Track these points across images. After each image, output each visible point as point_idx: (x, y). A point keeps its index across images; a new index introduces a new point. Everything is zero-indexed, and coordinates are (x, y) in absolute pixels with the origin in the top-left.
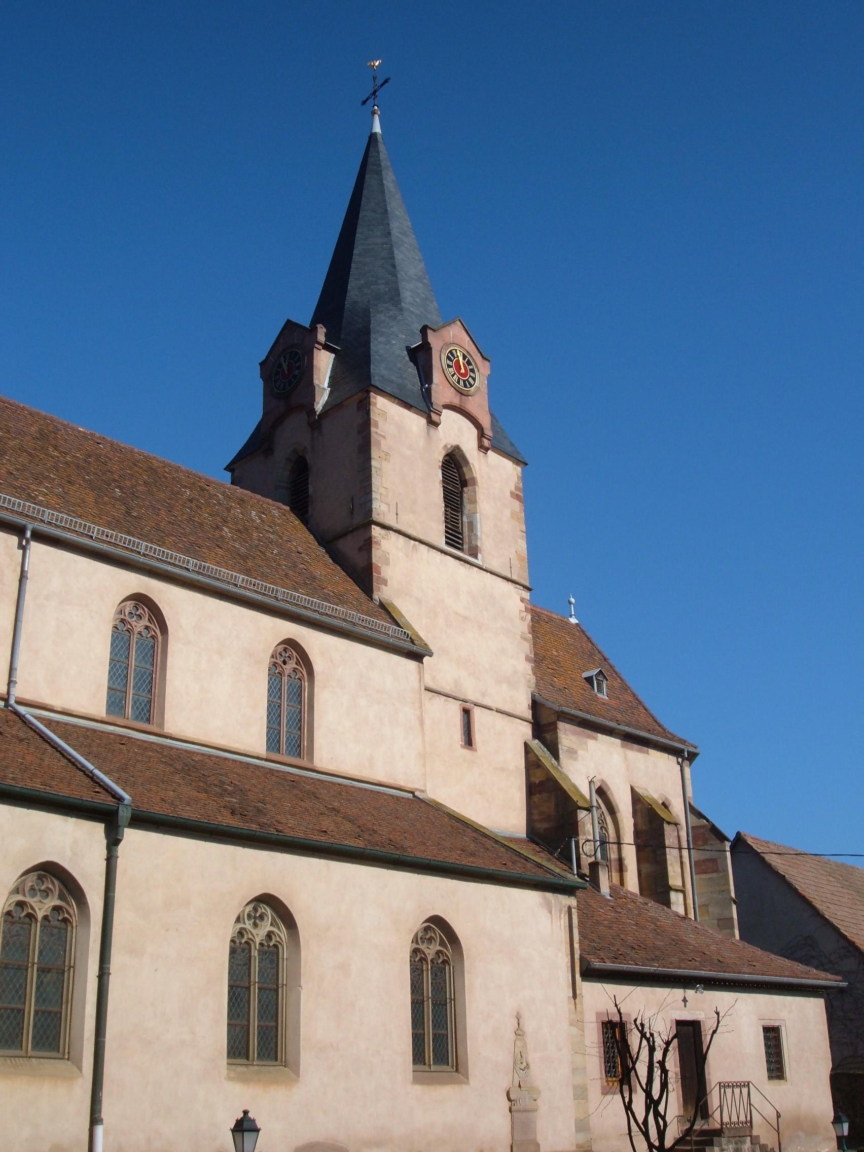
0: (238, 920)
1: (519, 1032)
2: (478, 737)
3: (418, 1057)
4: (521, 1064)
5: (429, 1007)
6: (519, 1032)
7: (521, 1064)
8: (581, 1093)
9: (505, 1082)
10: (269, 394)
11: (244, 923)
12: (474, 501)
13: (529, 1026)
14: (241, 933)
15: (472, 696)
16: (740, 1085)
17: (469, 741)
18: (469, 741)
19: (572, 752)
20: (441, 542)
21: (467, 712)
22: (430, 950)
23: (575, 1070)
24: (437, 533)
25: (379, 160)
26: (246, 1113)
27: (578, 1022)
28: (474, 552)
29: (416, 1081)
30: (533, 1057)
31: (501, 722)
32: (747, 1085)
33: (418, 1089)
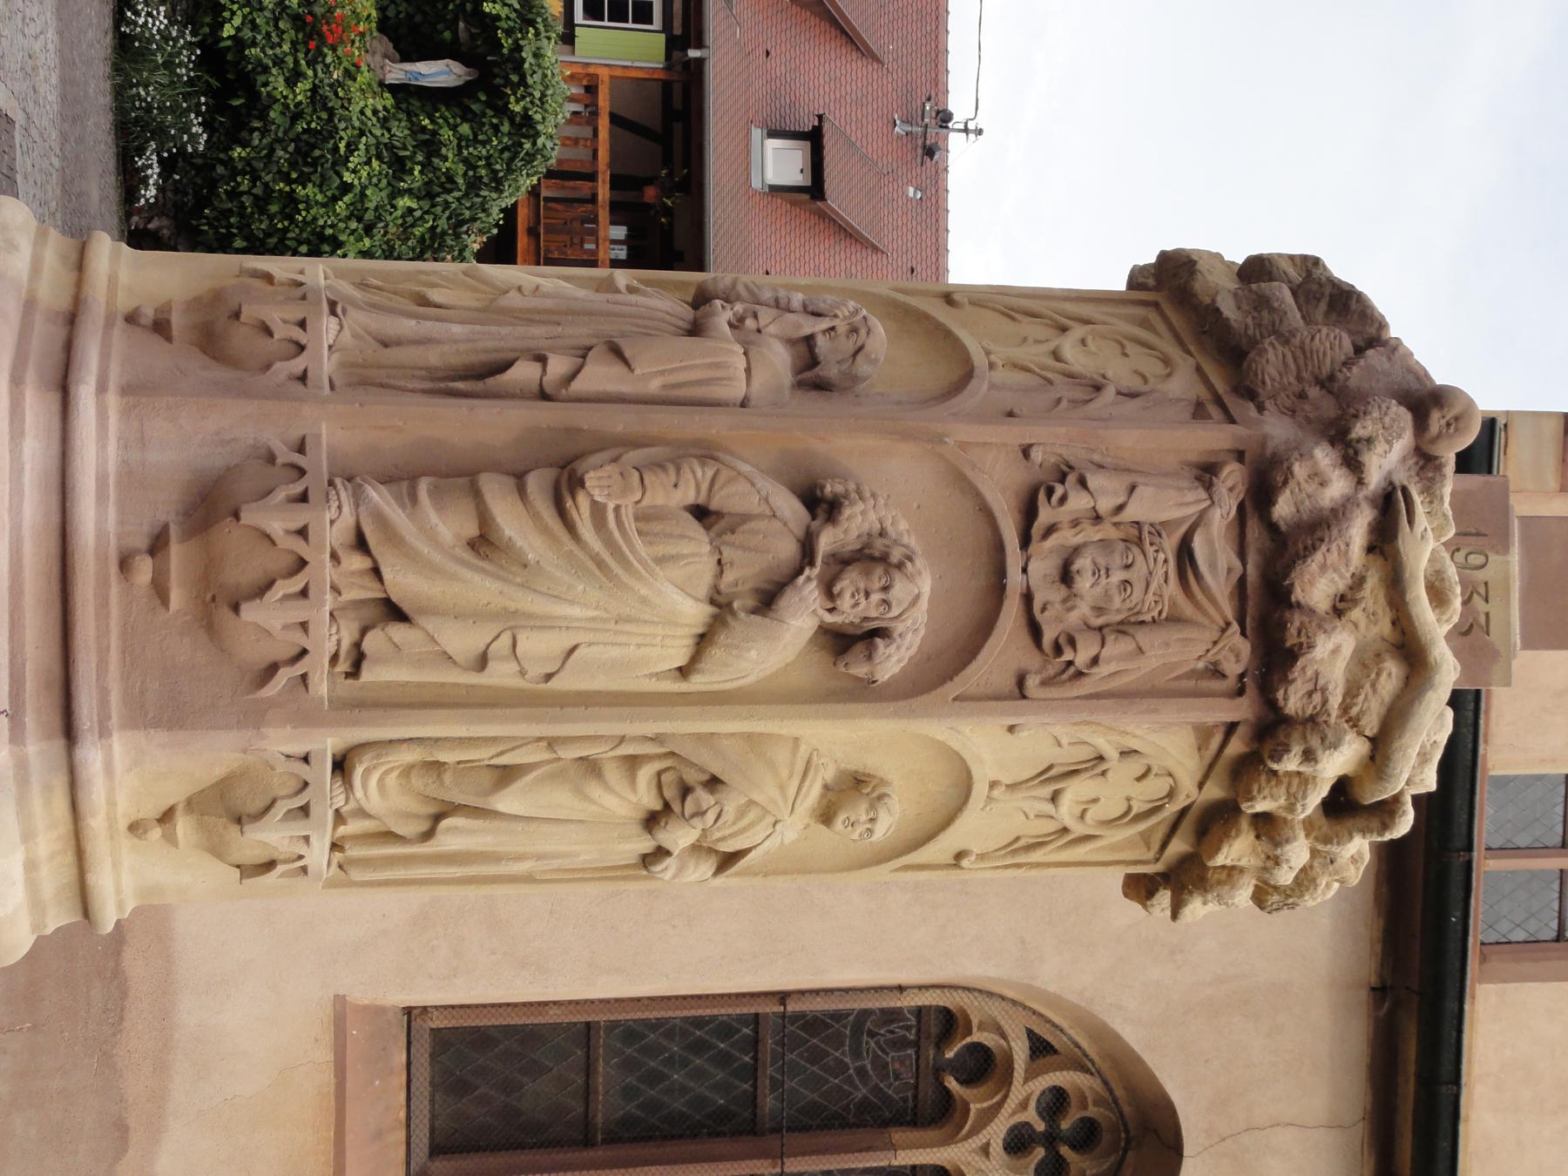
11: (1030, 1076)
14: (984, 1066)
29: (341, 1012)
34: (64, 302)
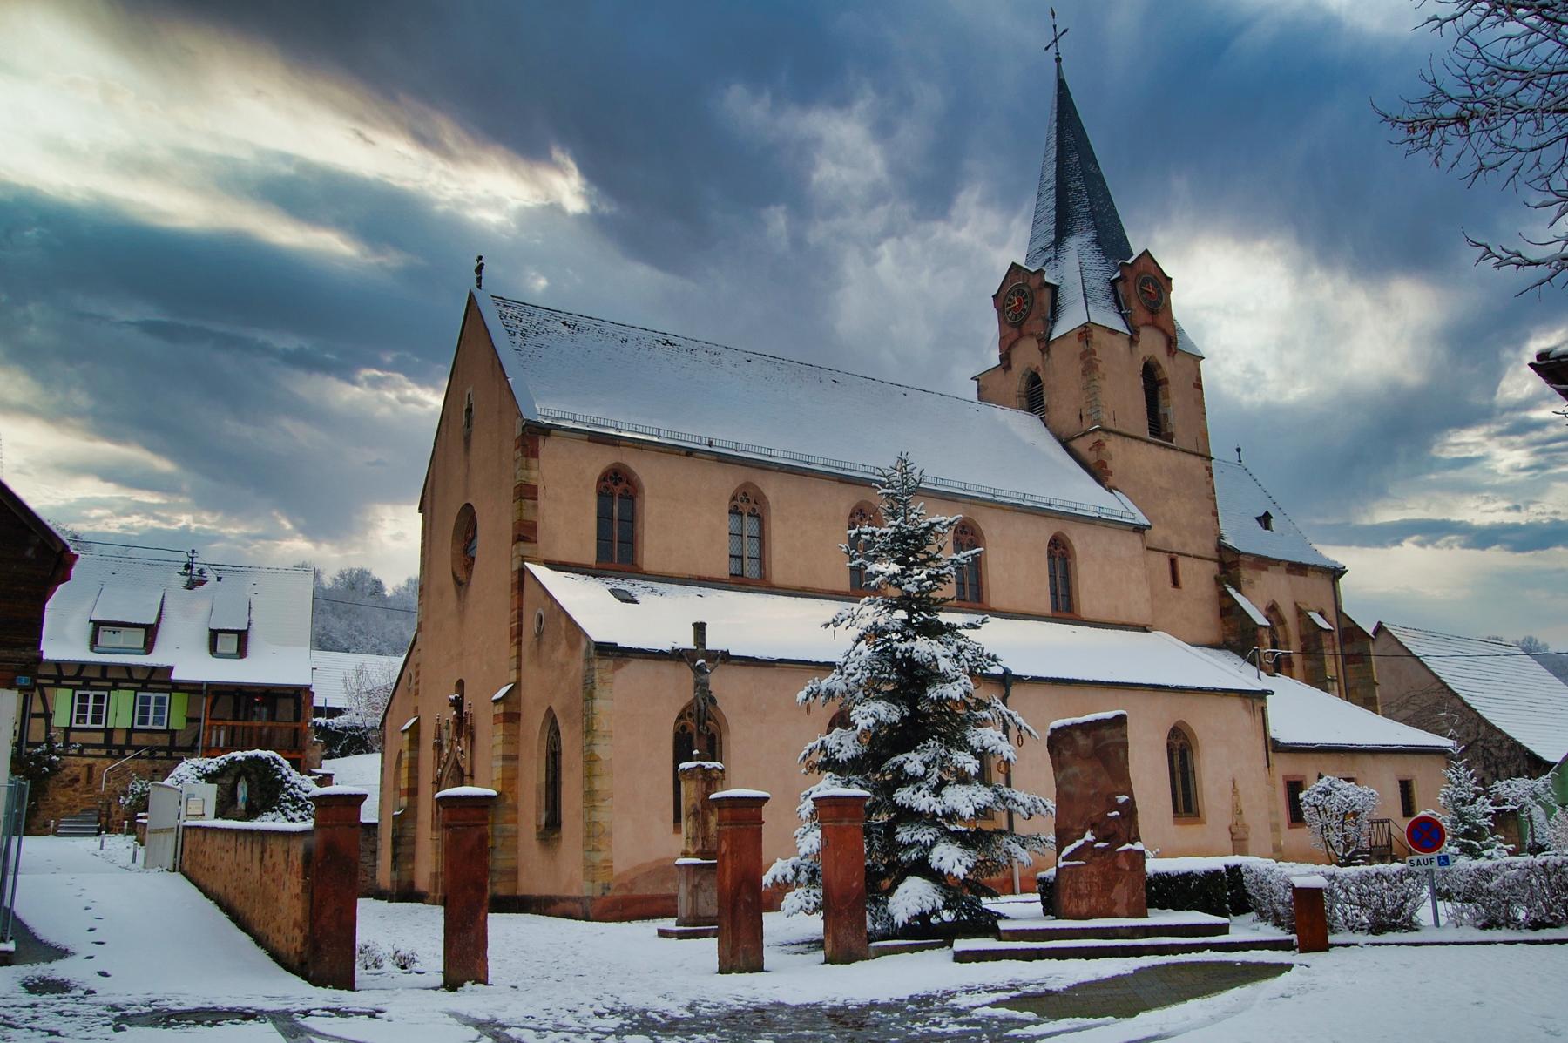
0: (681, 717)
1: (1235, 791)
2: (1182, 579)
3: (1175, 809)
4: (1237, 811)
5: (1178, 776)
6: (1235, 791)
7: (1237, 811)
8: (1275, 828)
9: (1228, 821)
10: (1002, 321)
12: (1167, 397)
13: (1240, 787)
14: (684, 728)
15: (1176, 547)
16: (1382, 821)
17: (1176, 582)
18: (1176, 582)
19: (1250, 582)
20: (1147, 436)
21: (1173, 562)
22: (1177, 744)
23: (1271, 813)
24: (1141, 426)
25: (486, 870)
26: (975, 378)
27: (1271, 784)
28: (1169, 437)
29: (1176, 823)
30: (1244, 806)
31: (1197, 564)
32: (1388, 821)
33: (1178, 827)
34: (1168, 1029)
